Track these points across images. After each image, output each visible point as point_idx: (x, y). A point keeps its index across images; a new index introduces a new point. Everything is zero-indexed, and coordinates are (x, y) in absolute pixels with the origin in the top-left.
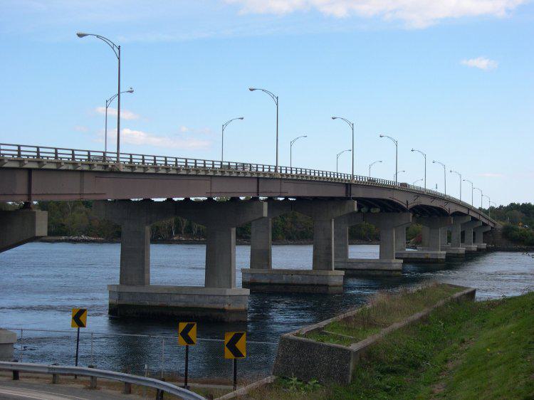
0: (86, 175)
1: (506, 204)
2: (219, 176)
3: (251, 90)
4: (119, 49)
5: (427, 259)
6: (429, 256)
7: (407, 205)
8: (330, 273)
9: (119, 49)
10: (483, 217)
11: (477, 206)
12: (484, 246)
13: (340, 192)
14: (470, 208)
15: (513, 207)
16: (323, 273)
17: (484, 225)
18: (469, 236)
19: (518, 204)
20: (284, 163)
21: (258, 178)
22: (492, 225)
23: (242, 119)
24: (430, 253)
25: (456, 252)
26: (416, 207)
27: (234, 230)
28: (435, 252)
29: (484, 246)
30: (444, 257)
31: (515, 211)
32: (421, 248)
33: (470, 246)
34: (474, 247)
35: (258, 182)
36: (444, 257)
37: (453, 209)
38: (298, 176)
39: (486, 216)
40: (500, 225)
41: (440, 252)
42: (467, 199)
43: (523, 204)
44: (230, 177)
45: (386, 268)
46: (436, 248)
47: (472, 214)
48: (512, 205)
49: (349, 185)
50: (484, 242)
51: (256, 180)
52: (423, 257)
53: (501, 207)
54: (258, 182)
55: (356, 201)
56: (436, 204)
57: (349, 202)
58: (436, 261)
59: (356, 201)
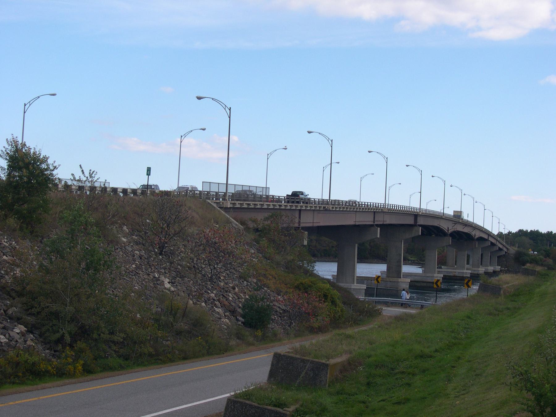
0: (316, 213)
1: (514, 230)
2: (265, 209)
3: (309, 132)
4: (230, 110)
5: (455, 276)
6: (457, 274)
7: (448, 231)
8: (400, 280)
9: (230, 110)
10: (499, 242)
11: (495, 232)
12: (498, 268)
13: (411, 221)
14: (489, 234)
15: (521, 233)
16: (395, 279)
17: (500, 249)
18: (487, 258)
19: (527, 231)
20: (423, 207)
21: (375, 212)
22: (505, 249)
23: (204, 129)
24: (457, 272)
25: (476, 273)
26: (454, 232)
27: (357, 245)
28: (461, 271)
29: (498, 268)
30: (469, 276)
31: (524, 238)
32: (446, 267)
33: (487, 268)
34: (491, 269)
35: (374, 214)
36: (469, 276)
37: (478, 234)
38: (363, 209)
39: (501, 241)
40: (513, 250)
41: (465, 271)
42: (488, 227)
43: (531, 231)
44: (261, 208)
45: (429, 281)
46: (463, 268)
47: (491, 239)
48: (521, 231)
49: (416, 215)
50: (498, 265)
51: (373, 214)
52: (452, 275)
53: (510, 233)
54: (374, 214)
55: (379, 229)
56: (466, 230)
57: (416, 228)
58: (462, 279)
59: (306, 233)
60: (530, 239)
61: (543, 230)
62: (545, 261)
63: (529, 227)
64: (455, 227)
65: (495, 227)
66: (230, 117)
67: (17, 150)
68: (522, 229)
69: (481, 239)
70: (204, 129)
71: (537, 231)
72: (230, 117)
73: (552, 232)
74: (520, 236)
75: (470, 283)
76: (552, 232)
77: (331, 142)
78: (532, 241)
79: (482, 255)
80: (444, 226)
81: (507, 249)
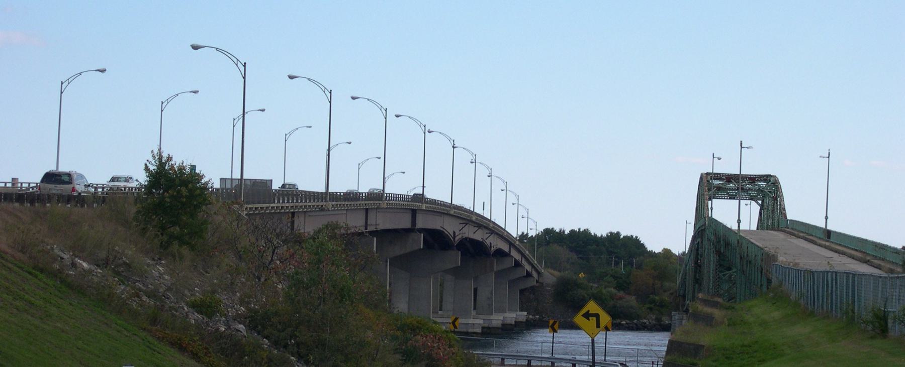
3: (353, 98)
4: (245, 66)
7: (454, 238)
9: (245, 66)
13: (404, 222)
19: (562, 233)
22: (535, 274)
29: (523, 316)
30: (479, 330)
31: (555, 247)
34: (497, 319)
36: (479, 330)
41: (471, 321)
43: (572, 231)
48: (548, 232)
50: (521, 310)
56: (478, 236)
60: (572, 249)
61: (600, 230)
62: (620, 298)
63: (566, 224)
64: (466, 230)
65: (516, 225)
66: (244, 78)
67: (161, 165)
68: (550, 227)
69: (500, 253)
70: (263, 110)
71: (586, 233)
72: (244, 78)
73: (618, 233)
74: (548, 243)
75: (556, 326)
76: (618, 233)
77: (329, 95)
78: (574, 256)
79: (476, 290)
80: (450, 227)
81: (539, 273)
